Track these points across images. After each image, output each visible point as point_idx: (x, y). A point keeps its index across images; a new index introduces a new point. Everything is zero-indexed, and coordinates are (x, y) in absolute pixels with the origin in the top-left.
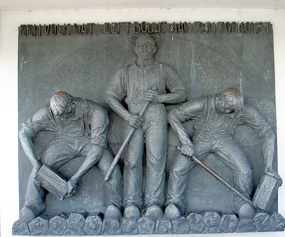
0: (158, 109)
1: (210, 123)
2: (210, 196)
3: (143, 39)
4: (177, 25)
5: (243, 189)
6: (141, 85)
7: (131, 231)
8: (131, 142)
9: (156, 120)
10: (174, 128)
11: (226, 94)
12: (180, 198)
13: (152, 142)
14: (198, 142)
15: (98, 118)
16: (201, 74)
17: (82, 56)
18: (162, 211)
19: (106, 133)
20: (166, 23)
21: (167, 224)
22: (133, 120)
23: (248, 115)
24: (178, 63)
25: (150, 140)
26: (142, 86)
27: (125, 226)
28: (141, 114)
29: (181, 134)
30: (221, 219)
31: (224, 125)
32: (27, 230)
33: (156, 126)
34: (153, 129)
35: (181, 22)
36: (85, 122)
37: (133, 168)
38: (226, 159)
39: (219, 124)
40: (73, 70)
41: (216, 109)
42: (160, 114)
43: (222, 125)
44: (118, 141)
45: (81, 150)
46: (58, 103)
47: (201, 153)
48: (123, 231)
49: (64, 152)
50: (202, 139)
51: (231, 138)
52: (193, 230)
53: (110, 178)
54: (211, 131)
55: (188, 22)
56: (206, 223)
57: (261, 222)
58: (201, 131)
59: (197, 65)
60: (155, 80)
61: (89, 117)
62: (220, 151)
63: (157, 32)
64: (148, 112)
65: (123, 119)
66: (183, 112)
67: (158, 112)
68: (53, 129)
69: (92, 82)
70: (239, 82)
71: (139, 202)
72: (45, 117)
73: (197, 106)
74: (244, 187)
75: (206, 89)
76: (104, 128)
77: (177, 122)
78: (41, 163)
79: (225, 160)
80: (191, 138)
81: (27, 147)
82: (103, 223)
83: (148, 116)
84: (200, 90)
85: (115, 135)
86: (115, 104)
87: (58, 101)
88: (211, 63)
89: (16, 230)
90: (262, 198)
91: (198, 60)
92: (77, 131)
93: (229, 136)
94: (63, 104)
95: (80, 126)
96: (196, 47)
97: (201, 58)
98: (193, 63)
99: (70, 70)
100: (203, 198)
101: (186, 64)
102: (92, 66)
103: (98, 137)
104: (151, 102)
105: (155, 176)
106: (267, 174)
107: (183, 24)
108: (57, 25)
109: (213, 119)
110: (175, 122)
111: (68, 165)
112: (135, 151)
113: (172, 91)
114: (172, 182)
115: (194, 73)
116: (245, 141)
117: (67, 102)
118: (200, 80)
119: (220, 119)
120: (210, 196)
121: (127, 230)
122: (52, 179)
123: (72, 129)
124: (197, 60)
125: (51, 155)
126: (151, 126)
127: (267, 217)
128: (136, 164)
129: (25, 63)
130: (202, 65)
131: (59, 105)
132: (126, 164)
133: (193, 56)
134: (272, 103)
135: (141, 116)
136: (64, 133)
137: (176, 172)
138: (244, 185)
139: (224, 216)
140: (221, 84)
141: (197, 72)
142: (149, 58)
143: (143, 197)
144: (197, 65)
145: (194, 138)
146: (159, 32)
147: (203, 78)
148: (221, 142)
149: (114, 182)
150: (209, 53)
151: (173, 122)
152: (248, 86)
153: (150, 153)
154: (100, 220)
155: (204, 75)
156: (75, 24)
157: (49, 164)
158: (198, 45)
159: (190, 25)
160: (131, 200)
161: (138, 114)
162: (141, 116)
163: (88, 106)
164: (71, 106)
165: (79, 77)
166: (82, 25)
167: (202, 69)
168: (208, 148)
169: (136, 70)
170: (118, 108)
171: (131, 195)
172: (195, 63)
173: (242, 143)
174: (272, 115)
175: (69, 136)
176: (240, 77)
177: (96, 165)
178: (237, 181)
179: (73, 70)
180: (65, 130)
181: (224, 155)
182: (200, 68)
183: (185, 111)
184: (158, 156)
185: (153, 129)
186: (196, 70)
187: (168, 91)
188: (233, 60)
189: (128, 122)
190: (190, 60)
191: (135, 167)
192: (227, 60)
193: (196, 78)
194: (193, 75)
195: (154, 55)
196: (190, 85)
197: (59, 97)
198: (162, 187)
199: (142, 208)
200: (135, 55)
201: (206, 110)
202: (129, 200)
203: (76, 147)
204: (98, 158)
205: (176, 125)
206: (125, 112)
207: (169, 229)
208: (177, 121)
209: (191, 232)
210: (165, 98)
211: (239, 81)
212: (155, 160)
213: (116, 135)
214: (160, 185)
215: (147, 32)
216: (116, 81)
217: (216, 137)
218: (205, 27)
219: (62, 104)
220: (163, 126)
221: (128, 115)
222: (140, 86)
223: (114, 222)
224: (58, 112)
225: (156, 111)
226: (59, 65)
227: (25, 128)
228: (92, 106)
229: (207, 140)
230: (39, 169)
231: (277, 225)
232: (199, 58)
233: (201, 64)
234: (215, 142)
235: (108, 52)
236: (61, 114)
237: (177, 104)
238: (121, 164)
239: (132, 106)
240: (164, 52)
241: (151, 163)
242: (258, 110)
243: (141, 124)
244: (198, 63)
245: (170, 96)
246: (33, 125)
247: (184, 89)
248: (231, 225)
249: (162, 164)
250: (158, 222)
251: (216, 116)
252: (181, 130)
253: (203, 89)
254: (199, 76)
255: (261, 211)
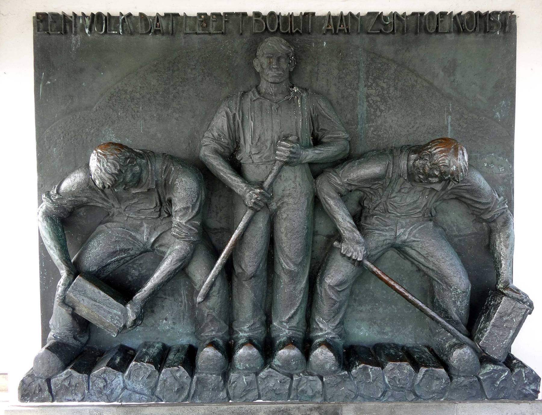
0: (298, 174)
1: (394, 197)
2: (387, 319)
3: (274, 44)
4: (335, 18)
5: (455, 316)
6: (268, 135)
7: (244, 396)
8: (247, 234)
9: (295, 195)
10: (326, 208)
11: (435, 152)
12: (336, 330)
13: (287, 234)
14: (371, 232)
15: (184, 190)
16: (377, 109)
17: (155, 74)
18: (303, 358)
19: (199, 216)
20: (313, 14)
21: (314, 383)
22: (251, 196)
23: (469, 184)
24: (333, 89)
25: (283, 230)
26: (270, 133)
27: (233, 385)
28: (266, 185)
29: (341, 220)
30: (416, 376)
31: (419, 201)
32: (47, 393)
33: (295, 204)
34: (288, 210)
35: (342, 12)
36: (161, 194)
37: (251, 278)
38: (422, 260)
39: (409, 200)
40: (138, 99)
41: (409, 175)
42: (301, 183)
43: (417, 200)
44: (223, 224)
45: (155, 242)
46: (103, 166)
47: (377, 251)
48: (231, 393)
49: (123, 246)
50: (377, 225)
51: (431, 223)
52: (362, 396)
53: (207, 297)
54: (395, 213)
55: (355, 13)
56: (388, 383)
57: (494, 382)
58: (375, 211)
59: (370, 91)
60: (296, 121)
61: (167, 186)
62: (411, 247)
63: (297, 32)
64: (279, 180)
65: (231, 191)
66: (346, 180)
67: (298, 179)
68: (103, 204)
69: (175, 121)
70: (446, 123)
71: (259, 333)
72: (83, 186)
73: (372, 169)
74: (456, 313)
75: (385, 136)
76: (196, 209)
77: (333, 198)
78: (75, 270)
79: (419, 262)
80: (359, 227)
81: (49, 240)
82: (192, 380)
83: (279, 188)
84: (374, 138)
85: (217, 213)
86: (217, 165)
87: (103, 162)
88: (396, 89)
89: (27, 392)
90: (489, 334)
91: (372, 84)
92: (146, 209)
93: (427, 221)
94: (113, 168)
95: (151, 202)
96: (369, 59)
97: (377, 80)
98: (363, 89)
99: (132, 99)
100: (375, 323)
101: (349, 90)
102: (174, 91)
103: (185, 226)
104: (286, 163)
105: (290, 291)
106: (505, 295)
107: (346, 17)
108: (106, 14)
109: (399, 191)
110: (330, 197)
111: (130, 265)
112: (255, 250)
113: (324, 140)
114: (322, 301)
115: (363, 106)
116: (454, 225)
117: (122, 164)
118: (375, 120)
119: (413, 191)
120: (387, 319)
121: (238, 391)
122: (94, 302)
123: (138, 206)
124: (369, 84)
125: (96, 253)
126: (285, 205)
127: (506, 374)
128: (256, 271)
129: (48, 85)
130: (379, 92)
131: (105, 169)
132: (238, 270)
133: (362, 75)
134: (507, 160)
135: (266, 189)
136: (123, 212)
137: (329, 285)
138: (457, 310)
139: (423, 370)
140: (413, 127)
141: (370, 106)
142: (282, 80)
143: (268, 323)
144: (370, 91)
145: (363, 224)
146: (301, 31)
147: (379, 116)
148: (414, 232)
149: (215, 300)
150: (392, 71)
151: (326, 197)
152: (462, 130)
153: (283, 251)
154: (187, 374)
155: (381, 111)
156: (141, 14)
157: (93, 270)
158: (372, 55)
159: (359, 19)
160: (245, 332)
161: (260, 185)
162: (266, 189)
163: (166, 168)
164: (131, 170)
165: (149, 113)
166: (155, 17)
167: (379, 99)
168: (388, 241)
169: (257, 103)
170: (222, 171)
171: (244, 323)
172: (366, 88)
173: (448, 230)
174: (506, 181)
175: (132, 218)
176: (450, 114)
177: (181, 271)
178: (443, 302)
179: (138, 99)
180: (123, 207)
181: (417, 254)
182: (375, 99)
183: (350, 178)
184: (298, 256)
185: (288, 210)
186: (368, 101)
187: (317, 142)
188: (436, 83)
189: (242, 198)
190: (357, 84)
191: (253, 276)
192: (425, 84)
193: (367, 117)
194: (362, 109)
195: (291, 75)
196: (356, 128)
197: (104, 155)
198: (303, 309)
199: (267, 348)
200: (254, 75)
201: (391, 176)
202: (241, 331)
203: (146, 236)
204: (184, 262)
205: (331, 202)
206: (236, 179)
207: (316, 392)
208: (334, 195)
209: (359, 398)
210: (311, 154)
211: (447, 120)
212: (292, 265)
213: (219, 215)
214: (299, 307)
215: (277, 31)
216: (220, 122)
217: (404, 222)
218: (387, 22)
219: (110, 168)
220: (308, 203)
221: (243, 185)
222: (266, 132)
223: (213, 379)
224: (103, 183)
225: (295, 177)
226: (113, 90)
227: (46, 204)
228: (173, 169)
229: (387, 228)
230: (70, 284)
231: (526, 390)
232: (374, 80)
233: (377, 91)
234: (402, 230)
235: (203, 68)
236: (109, 186)
237: (336, 163)
238: (229, 271)
239: (251, 171)
240: (309, 68)
241: (283, 269)
242: (482, 173)
243: (268, 208)
244: (372, 89)
245: (321, 151)
246: (62, 198)
247: (347, 136)
248: (436, 385)
249: (303, 270)
250: (295, 378)
251: (406, 186)
252: (342, 213)
253: (380, 136)
254: (372, 113)
255: (494, 362)
